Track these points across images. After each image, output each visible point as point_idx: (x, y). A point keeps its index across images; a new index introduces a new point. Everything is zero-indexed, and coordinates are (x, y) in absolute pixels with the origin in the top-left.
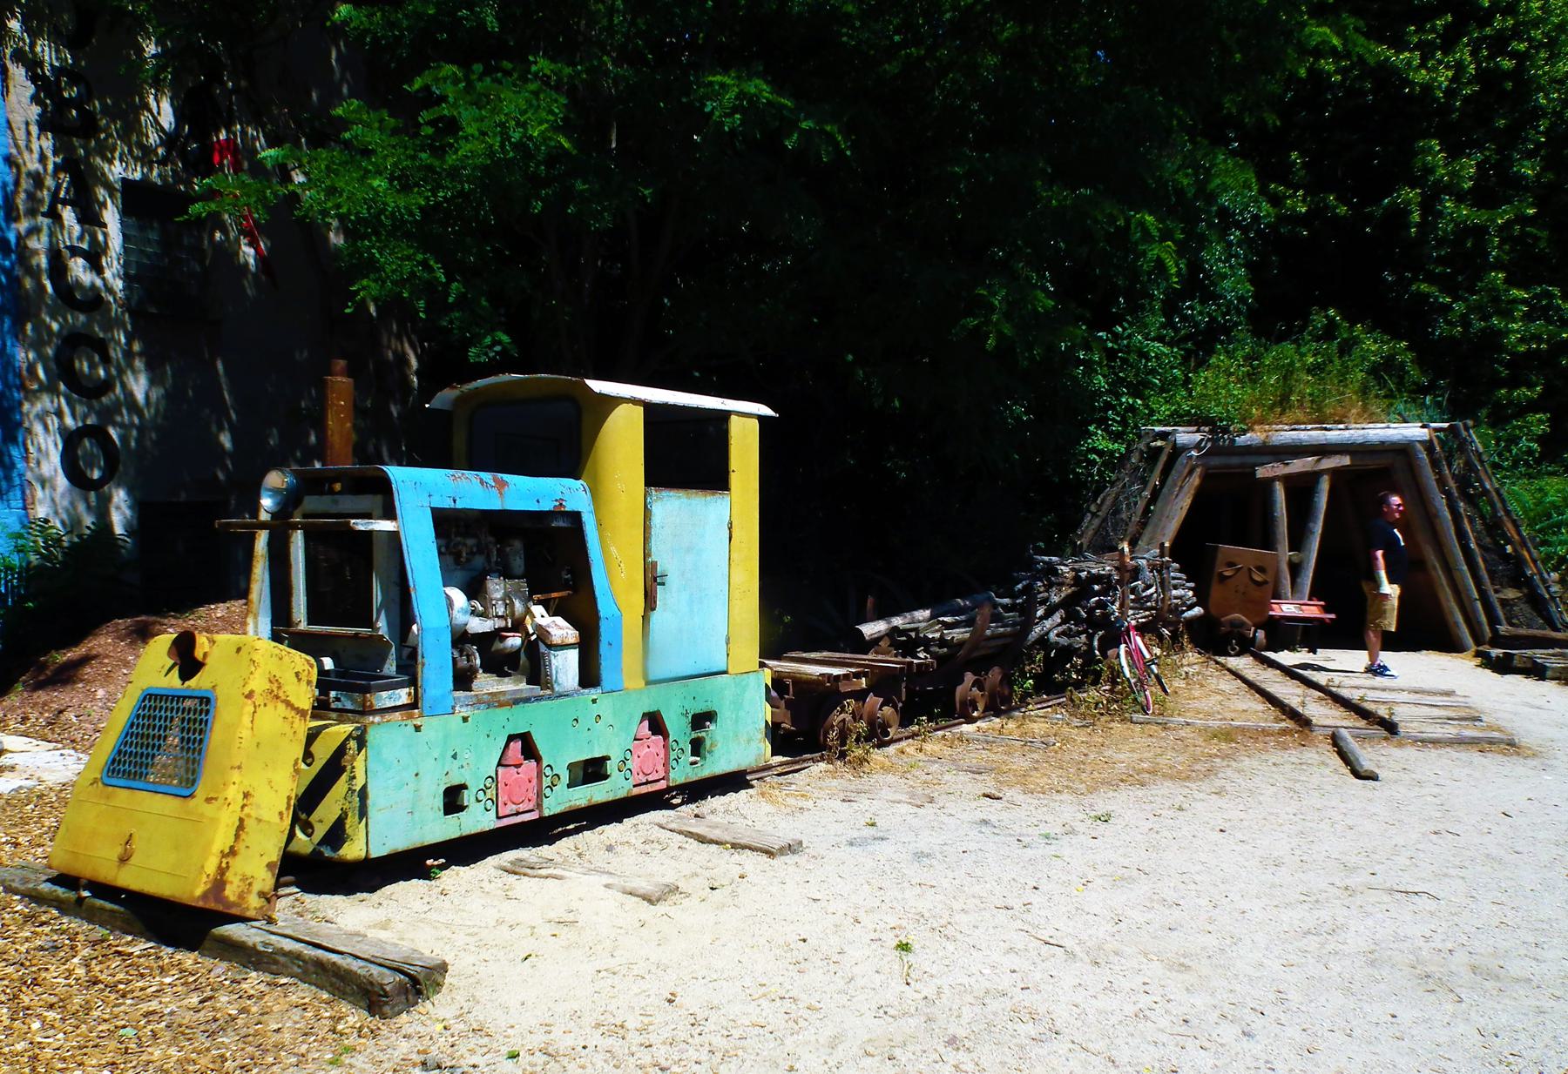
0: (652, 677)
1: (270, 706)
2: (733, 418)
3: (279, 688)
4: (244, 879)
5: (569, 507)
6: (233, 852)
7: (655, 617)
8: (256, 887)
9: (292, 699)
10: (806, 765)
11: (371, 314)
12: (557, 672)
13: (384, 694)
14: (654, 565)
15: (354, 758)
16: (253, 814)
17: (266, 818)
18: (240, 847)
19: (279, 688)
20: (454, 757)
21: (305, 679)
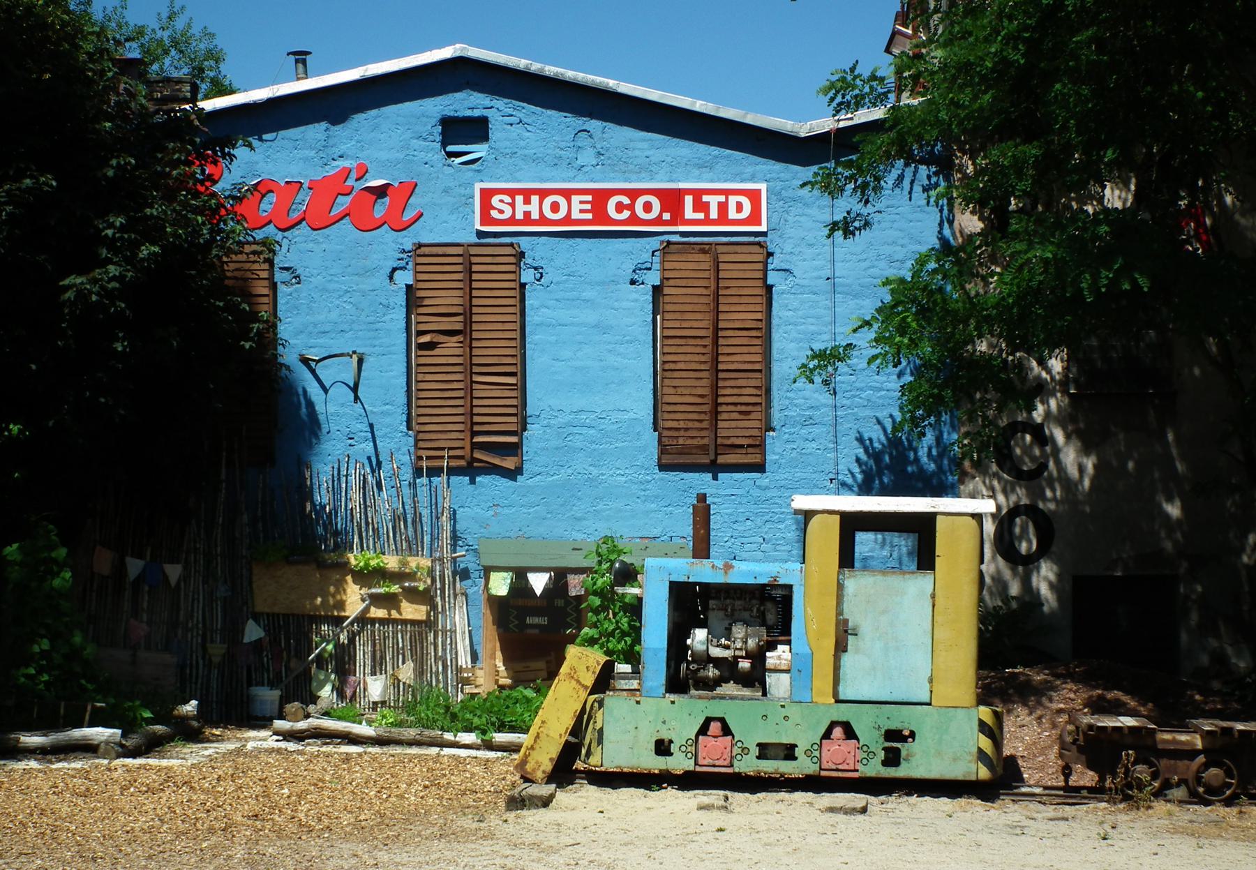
0: (842, 697)
1: (567, 682)
2: (939, 518)
3: (575, 673)
4: (537, 762)
5: (781, 581)
6: (532, 748)
7: (846, 659)
8: (542, 768)
9: (581, 680)
10: (1086, 801)
11: (1141, 274)
12: (770, 686)
13: (623, 682)
14: (846, 621)
15: (596, 713)
16: (545, 732)
17: (551, 735)
18: (537, 746)
19: (575, 673)
20: (664, 722)
21: (591, 670)
